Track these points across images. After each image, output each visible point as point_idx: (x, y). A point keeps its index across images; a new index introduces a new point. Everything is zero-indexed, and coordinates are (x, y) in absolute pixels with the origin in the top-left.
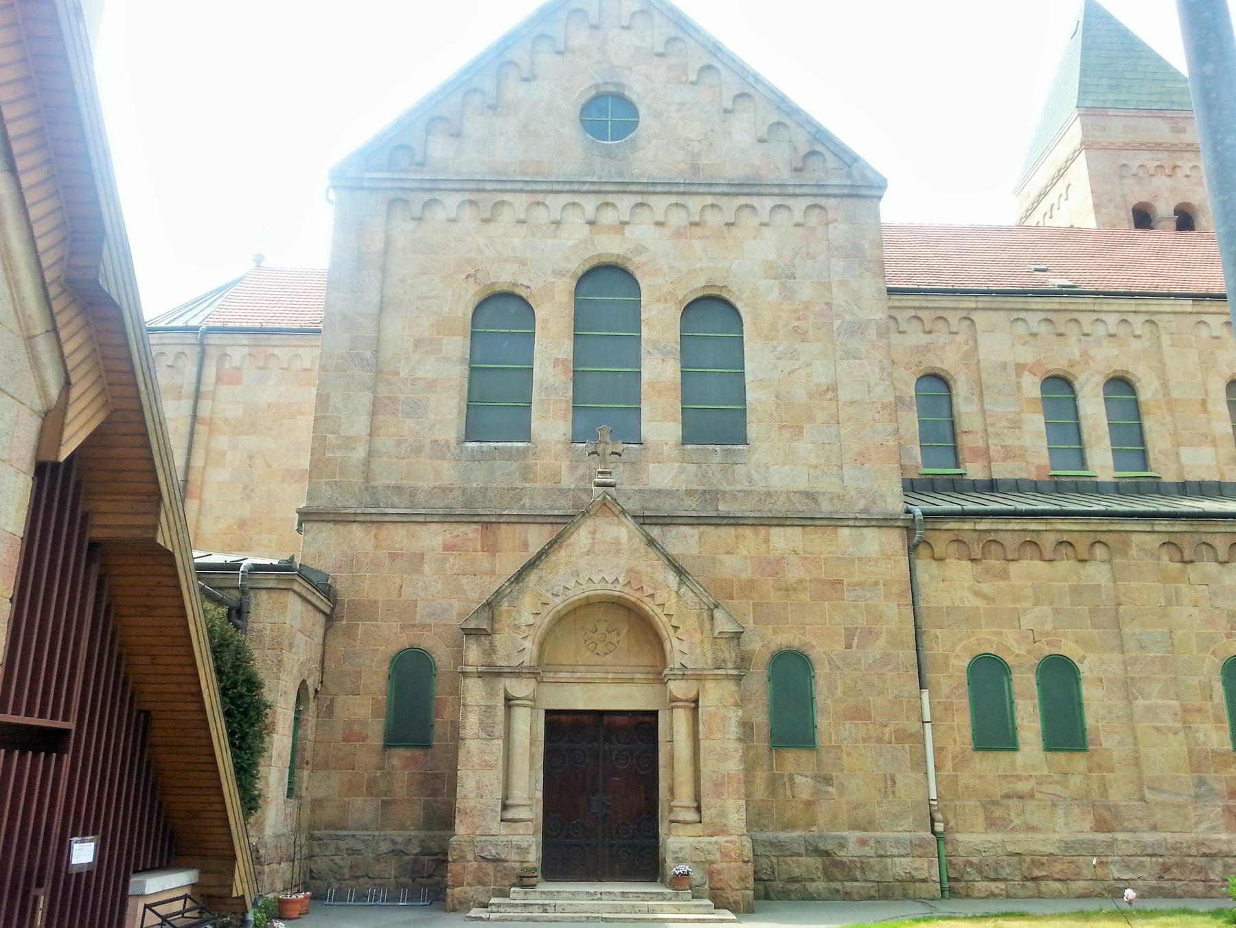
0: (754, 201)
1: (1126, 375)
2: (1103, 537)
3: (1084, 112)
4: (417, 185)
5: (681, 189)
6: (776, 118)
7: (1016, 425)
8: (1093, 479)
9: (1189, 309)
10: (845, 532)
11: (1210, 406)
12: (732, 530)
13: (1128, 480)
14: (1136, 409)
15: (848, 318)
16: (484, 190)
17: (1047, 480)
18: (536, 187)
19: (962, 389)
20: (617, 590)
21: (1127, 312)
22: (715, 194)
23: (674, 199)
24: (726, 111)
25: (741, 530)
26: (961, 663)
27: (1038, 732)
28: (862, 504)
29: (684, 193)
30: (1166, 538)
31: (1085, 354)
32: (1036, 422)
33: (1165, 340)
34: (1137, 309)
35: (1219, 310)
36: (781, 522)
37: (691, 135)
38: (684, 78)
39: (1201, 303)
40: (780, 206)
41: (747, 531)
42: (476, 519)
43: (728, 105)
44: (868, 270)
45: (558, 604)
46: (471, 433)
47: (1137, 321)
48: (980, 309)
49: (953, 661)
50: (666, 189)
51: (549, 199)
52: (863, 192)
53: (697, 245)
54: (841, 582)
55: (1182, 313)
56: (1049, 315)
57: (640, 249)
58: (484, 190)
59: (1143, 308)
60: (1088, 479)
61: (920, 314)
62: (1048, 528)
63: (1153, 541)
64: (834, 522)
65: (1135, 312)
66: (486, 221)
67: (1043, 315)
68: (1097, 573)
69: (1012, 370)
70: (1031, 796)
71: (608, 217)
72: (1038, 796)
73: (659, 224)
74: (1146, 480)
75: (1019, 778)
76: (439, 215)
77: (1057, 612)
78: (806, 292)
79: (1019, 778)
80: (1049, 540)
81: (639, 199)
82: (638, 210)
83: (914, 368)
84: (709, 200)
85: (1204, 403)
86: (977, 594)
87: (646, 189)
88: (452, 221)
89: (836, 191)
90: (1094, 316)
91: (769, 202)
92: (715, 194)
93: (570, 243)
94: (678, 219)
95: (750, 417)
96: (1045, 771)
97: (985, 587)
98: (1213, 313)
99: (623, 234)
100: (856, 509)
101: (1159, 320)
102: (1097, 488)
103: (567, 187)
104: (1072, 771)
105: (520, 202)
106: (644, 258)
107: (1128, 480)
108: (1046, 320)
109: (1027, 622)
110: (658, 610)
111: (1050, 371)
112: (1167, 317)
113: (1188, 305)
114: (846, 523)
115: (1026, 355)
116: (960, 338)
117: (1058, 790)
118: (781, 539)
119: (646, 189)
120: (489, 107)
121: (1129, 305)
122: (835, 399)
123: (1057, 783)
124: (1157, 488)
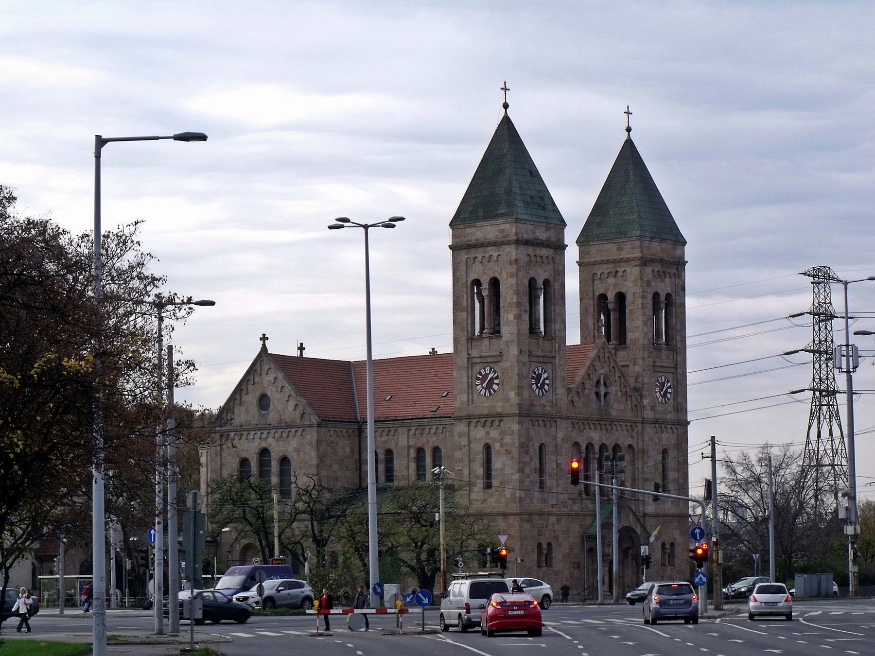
32: (413, 466)
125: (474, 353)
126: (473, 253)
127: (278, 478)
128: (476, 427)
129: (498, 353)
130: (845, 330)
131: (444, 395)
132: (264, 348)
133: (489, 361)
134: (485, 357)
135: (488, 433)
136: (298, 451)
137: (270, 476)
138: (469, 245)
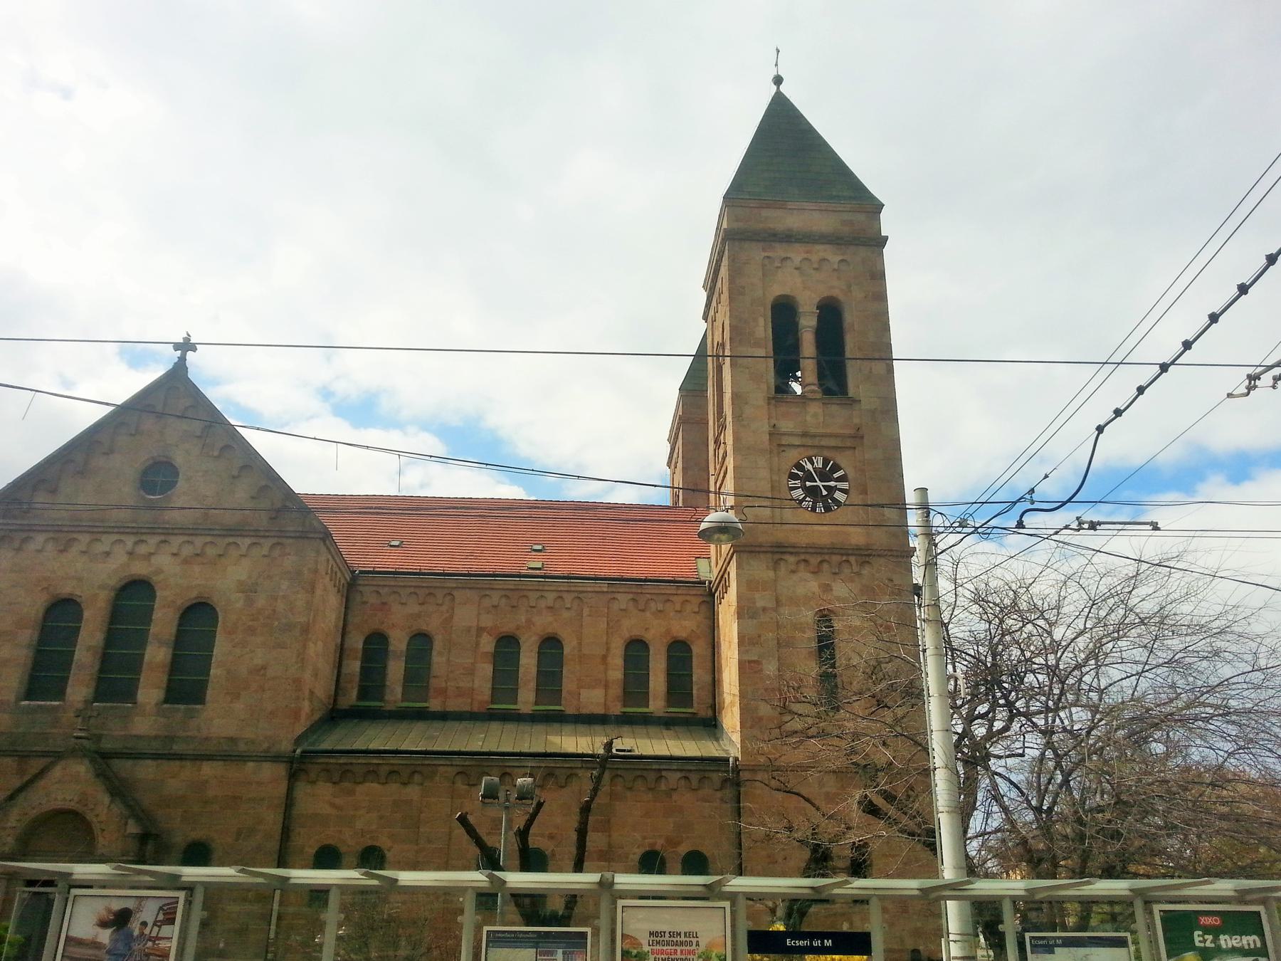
0: (239, 540)
1: (555, 636)
2: (418, 769)
4: (18, 527)
5: (191, 532)
6: (263, 483)
7: (471, 672)
8: (517, 711)
10: (251, 764)
12: (178, 763)
14: (559, 661)
15: (284, 621)
16: (61, 531)
18: (95, 530)
19: (438, 645)
20: (72, 806)
22: (213, 535)
23: (186, 538)
24: (234, 477)
25: (184, 763)
28: (265, 745)
29: (192, 535)
30: (460, 769)
31: (529, 621)
32: (486, 669)
33: (586, 611)
34: (569, 589)
36: (209, 758)
37: (207, 493)
38: (211, 453)
40: (254, 544)
41: (188, 764)
42: (15, 754)
43: (235, 473)
44: (303, 588)
45: (34, 813)
46: (30, 694)
47: (568, 598)
48: (459, 588)
49: (631, 856)
50: (181, 531)
51: (104, 537)
53: (197, 569)
54: (241, 798)
55: (600, 592)
56: (507, 593)
57: (159, 571)
58: (61, 531)
60: (513, 712)
61: (417, 591)
63: (452, 771)
64: (242, 758)
65: (568, 591)
66: (61, 551)
67: (503, 593)
68: (413, 792)
69: (474, 632)
71: (143, 549)
73: (174, 555)
76: (32, 546)
77: (381, 818)
78: (261, 602)
80: (384, 771)
81: (163, 538)
82: (163, 545)
84: (209, 539)
85: (604, 658)
86: (333, 805)
87: (168, 532)
88: (39, 551)
89: (292, 535)
90: (539, 594)
91: (248, 541)
92: (213, 535)
93: (114, 566)
94: (187, 551)
95: (210, 685)
97: (338, 801)
99: (149, 561)
100: (261, 749)
103: (116, 530)
105: (85, 538)
106: (161, 577)
108: (505, 596)
109: (359, 825)
110: (94, 820)
111: (504, 632)
113: (604, 586)
114: (251, 759)
115: (487, 621)
116: (444, 608)
118: (208, 769)
119: (168, 532)
120: (78, 473)
122: (264, 675)
125: (786, 425)
126: (780, 251)
127: (170, 651)
128: (793, 572)
129: (852, 432)
130: (668, 753)
131: (393, 543)
132: (180, 367)
133: (823, 443)
134: (814, 436)
135: (827, 588)
136: (249, 590)
137: (143, 644)
138: (775, 235)
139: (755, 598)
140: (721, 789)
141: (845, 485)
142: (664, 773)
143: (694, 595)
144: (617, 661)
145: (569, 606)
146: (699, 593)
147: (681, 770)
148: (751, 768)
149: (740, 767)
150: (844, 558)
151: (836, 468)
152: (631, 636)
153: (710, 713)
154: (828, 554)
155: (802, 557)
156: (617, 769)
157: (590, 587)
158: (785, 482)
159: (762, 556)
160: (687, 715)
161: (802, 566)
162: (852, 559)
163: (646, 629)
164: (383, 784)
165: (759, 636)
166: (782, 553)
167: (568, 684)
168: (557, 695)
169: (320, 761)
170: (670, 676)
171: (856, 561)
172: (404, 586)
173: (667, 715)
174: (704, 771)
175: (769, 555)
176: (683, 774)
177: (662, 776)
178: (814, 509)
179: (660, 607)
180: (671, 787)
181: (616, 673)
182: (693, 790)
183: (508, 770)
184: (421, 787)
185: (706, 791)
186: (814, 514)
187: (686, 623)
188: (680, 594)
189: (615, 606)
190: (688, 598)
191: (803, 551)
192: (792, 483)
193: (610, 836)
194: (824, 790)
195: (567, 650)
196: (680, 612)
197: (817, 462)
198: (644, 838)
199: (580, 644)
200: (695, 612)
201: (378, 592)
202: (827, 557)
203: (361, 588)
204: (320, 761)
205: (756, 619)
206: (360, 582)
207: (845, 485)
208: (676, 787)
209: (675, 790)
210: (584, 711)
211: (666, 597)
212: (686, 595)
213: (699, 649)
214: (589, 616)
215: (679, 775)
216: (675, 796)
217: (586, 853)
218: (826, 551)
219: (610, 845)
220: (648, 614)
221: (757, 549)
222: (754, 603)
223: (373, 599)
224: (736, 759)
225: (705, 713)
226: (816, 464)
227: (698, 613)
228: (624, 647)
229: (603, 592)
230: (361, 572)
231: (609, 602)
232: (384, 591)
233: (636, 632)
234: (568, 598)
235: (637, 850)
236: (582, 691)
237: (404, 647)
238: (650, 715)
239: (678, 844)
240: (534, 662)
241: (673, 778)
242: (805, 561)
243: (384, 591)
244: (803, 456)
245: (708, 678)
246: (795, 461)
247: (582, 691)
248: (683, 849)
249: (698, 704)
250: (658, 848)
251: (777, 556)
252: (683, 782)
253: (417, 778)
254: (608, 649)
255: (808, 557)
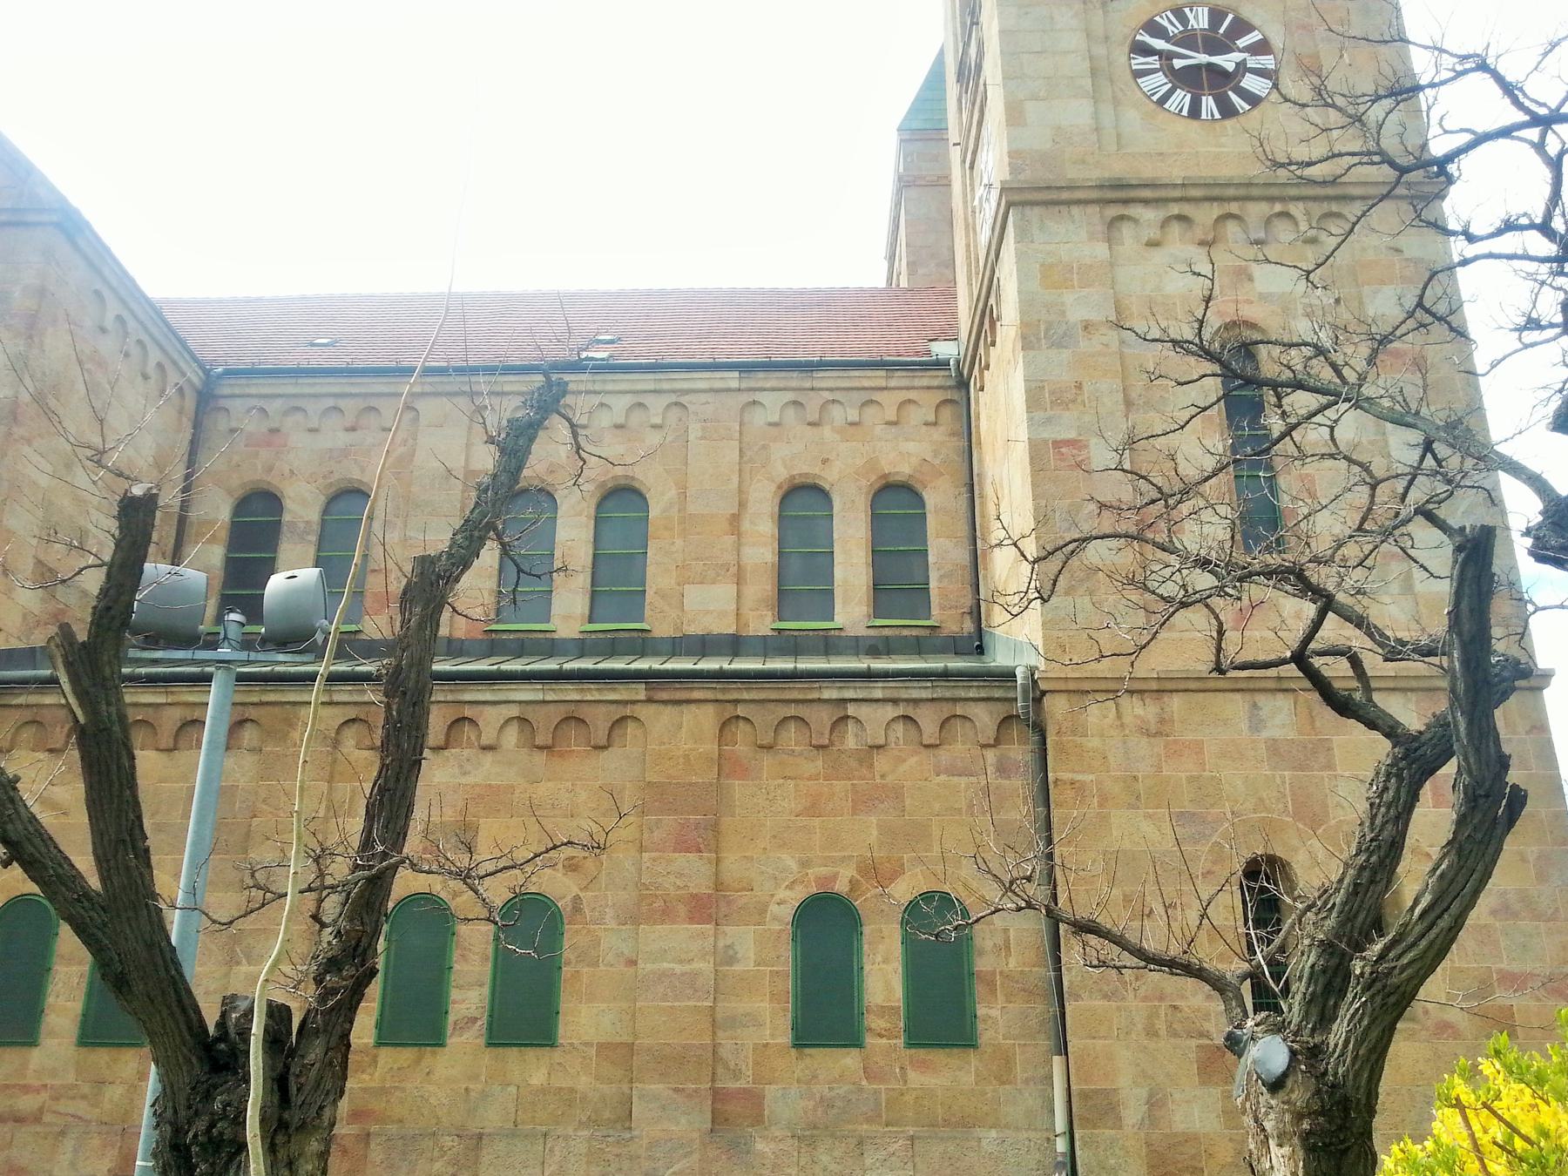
3: (908, 137)
8: (548, 635)
9: (734, 384)
11: (746, 526)
13: (601, 636)
17: (480, 637)
21: (645, 392)
26: (785, 903)
27: (76, 1016)
30: (352, 713)
33: (695, 431)
34: (658, 386)
35: (781, 384)
39: (752, 375)
49: (773, 908)
52: (31, 218)
59: (666, 386)
61: (342, 403)
62: (169, 701)
70: (37, 1118)
72: (47, 1118)
74: (627, 635)
75: (26, 1089)
79: (26, 1089)
83: (321, 480)
85: (735, 520)
96: (70, 1078)
98: (773, 389)
101: (691, 402)
102: (552, 647)
104: (111, 1080)
107: (601, 636)
112: (703, 398)
113: (732, 379)
117: (81, 1108)
121: (646, 381)
123: (84, 1097)
124: (643, 644)
128: (1153, 244)
139: (1063, 304)
140: (997, 742)
141: (1267, 62)
142: (851, 710)
143: (923, 388)
144: (762, 528)
145: (657, 420)
146: (936, 383)
147: (895, 701)
148: (1072, 686)
149: (1043, 686)
150: (1278, 207)
151: (1241, 27)
152: (793, 477)
153: (969, 626)
154: (1236, 199)
155: (1175, 209)
156: (736, 702)
157: (701, 380)
158: (1124, 59)
159: (1075, 210)
160: (915, 632)
161: (1176, 229)
162: (1296, 209)
163: (825, 461)
164: (169, 750)
165: (1079, 386)
166: (1126, 202)
167: (658, 576)
168: (634, 601)
169: (21, 700)
170: (878, 556)
171: (1307, 213)
172: (315, 396)
173: (872, 632)
174: (955, 700)
175: (1093, 210)
176: (901, 710)
177: (848, 717)
178: (1195, 112)
179: (853, 415)
180: (870, 742)
181: (761, 550)
182: (927, 746)
183: (468, 712)
184: (256, 757)
185: (959, 749)
186: (1195, 123)
187: (911, 447)
188: (894, 389)
189: (758, 418)
190: (912, 395)
191: (1177, 193)
192: (1139, 62)
193: (718, 861)
194: (1265, 734)
195: (654, 512)
196: (895, 423)
197: (1196, 18)
198: (805, 864)
199: (683, 495)
200: (926, 424)
201: (263, 410)
202: (1234, 208)
203: (223, 403)
204: (21, 700)
205: (1066, 347)
206: (226, 391)
207: (1267, 62)
208: (882, 742)
209: (879, 747)
210: (693, 629)
211: (865, 396)
212: (908, 388)
213: (939, 499)
214: (702, 438)
215: (890, 712)
216: (881, 762)
217: (158, 514)
218: (1231, 192)
219: (719, 885)
220: (826, 431)
221: (1065, 195)
222: (1063, 313)
223: (252, 425)
224: (1032, 670)
225: (954, 624)
226: (1192, 21)
227: (935, 424)
228: (777, 500)
229: (728, 390)
230: (229, 373)
231: (743, 409)
232: (274, 406)
233: (805, 468)
234: (657, 404)
235: (782, 894)
236: (689, 590)
237: (314, 515)
238: (837, 633)
239: (895, 874)
240: (587, 534)
241: (875, 719)
242: (1182, 218)
243: (274, 406)
244: (1162, 6)
245: (963, 556)
246: (1145, 18)
247: (689, 590)
248: (904, 890)
249: (942, 608)
250: (841, 887)
251: (1113, 211)
252: (899, 728)
253: (249, 735)
254: (742, 505)
255: (1187, 209)
